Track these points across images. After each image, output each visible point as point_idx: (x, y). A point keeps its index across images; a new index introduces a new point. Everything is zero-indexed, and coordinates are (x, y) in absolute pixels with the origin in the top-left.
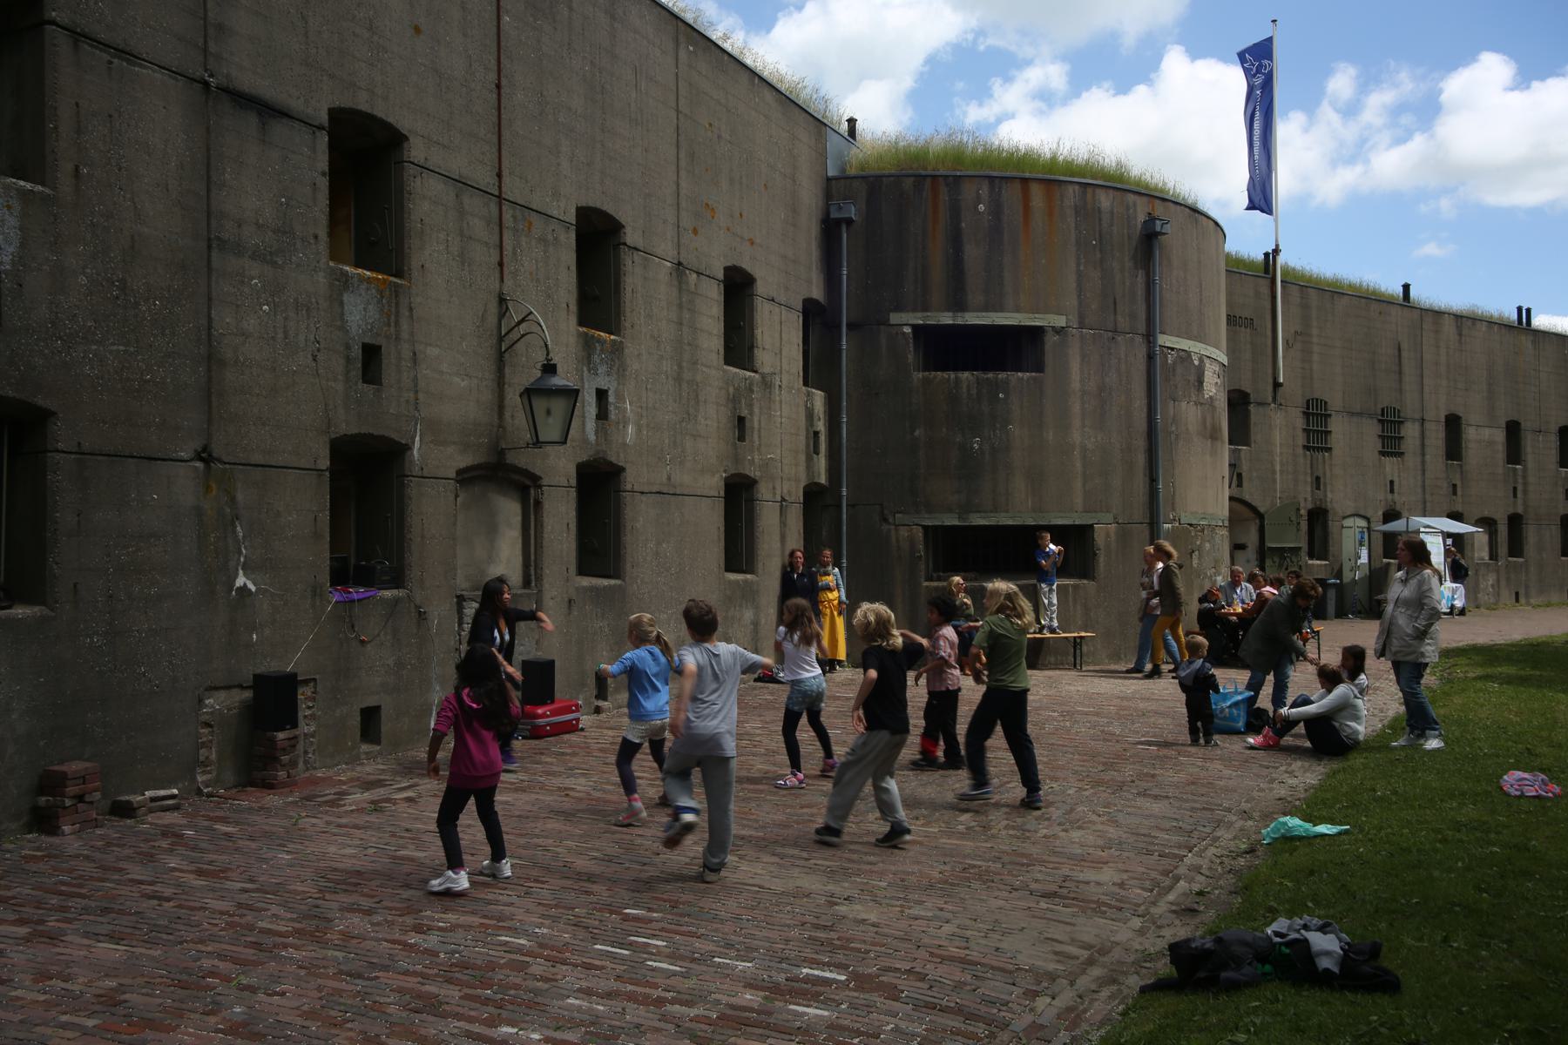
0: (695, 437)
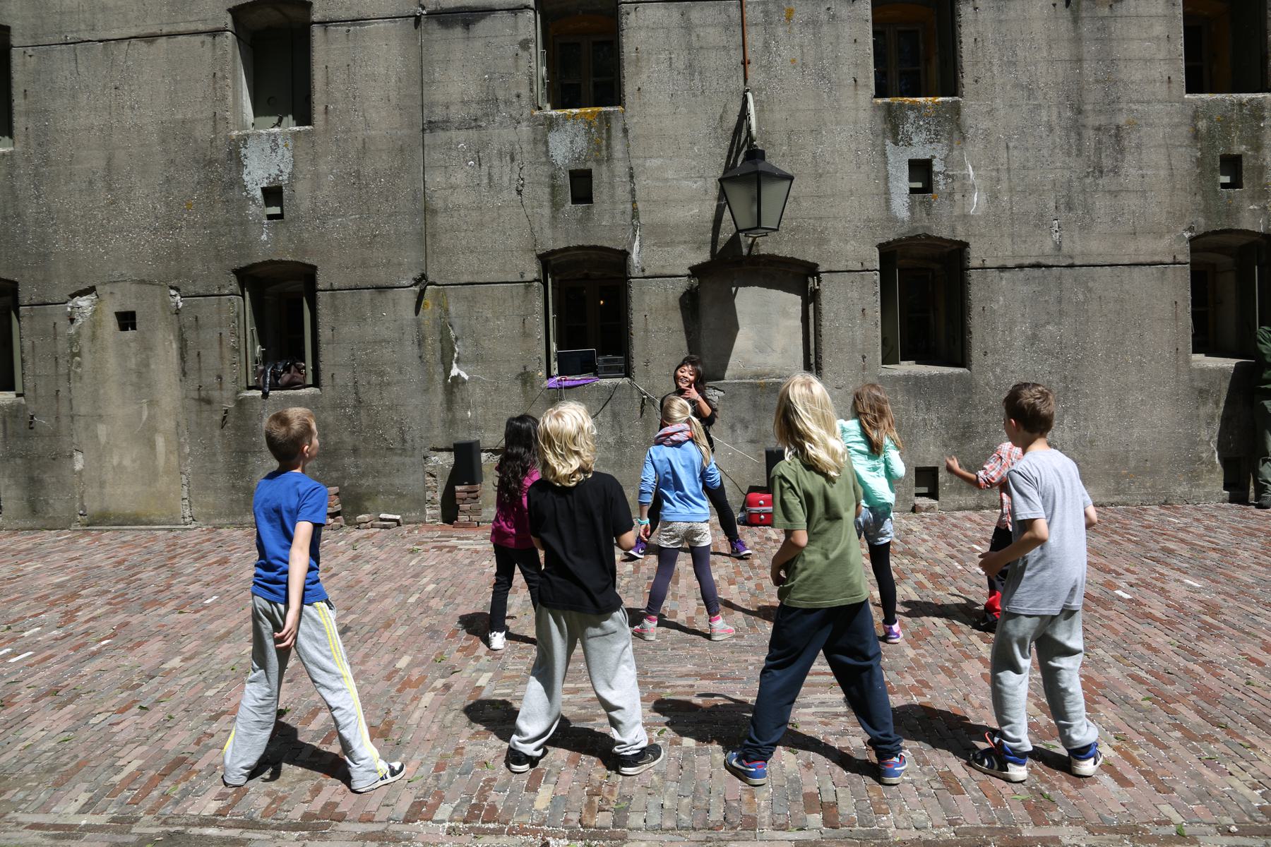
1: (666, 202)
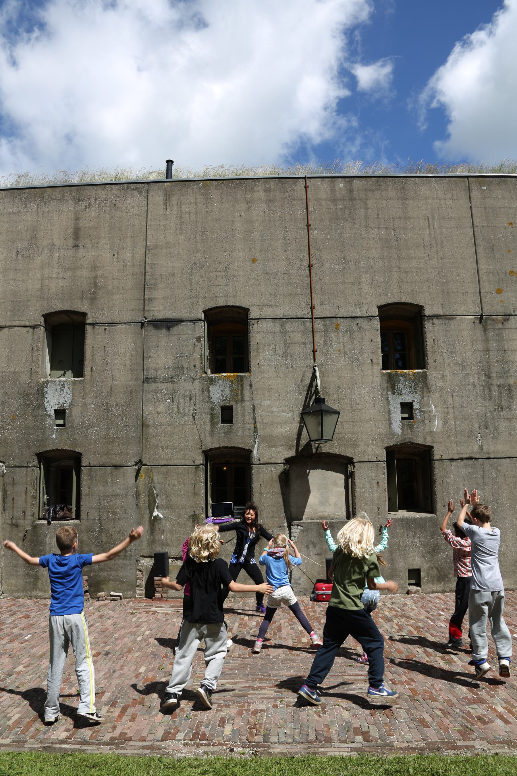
1: (272, 424)
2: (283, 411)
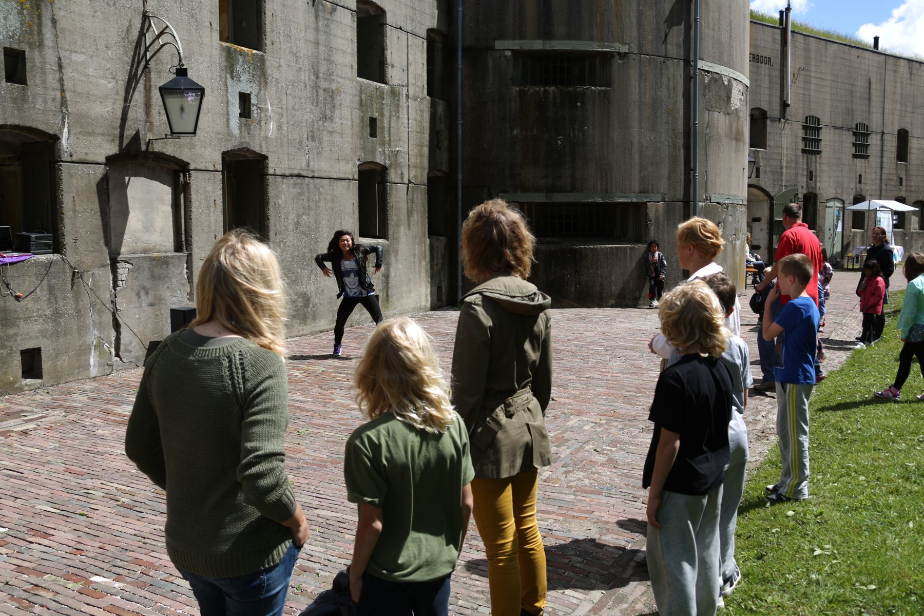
0: (331, 133)
2: (104, 77)
